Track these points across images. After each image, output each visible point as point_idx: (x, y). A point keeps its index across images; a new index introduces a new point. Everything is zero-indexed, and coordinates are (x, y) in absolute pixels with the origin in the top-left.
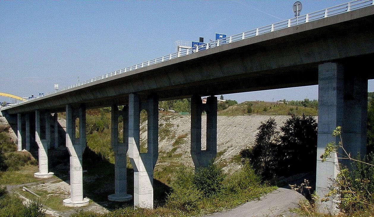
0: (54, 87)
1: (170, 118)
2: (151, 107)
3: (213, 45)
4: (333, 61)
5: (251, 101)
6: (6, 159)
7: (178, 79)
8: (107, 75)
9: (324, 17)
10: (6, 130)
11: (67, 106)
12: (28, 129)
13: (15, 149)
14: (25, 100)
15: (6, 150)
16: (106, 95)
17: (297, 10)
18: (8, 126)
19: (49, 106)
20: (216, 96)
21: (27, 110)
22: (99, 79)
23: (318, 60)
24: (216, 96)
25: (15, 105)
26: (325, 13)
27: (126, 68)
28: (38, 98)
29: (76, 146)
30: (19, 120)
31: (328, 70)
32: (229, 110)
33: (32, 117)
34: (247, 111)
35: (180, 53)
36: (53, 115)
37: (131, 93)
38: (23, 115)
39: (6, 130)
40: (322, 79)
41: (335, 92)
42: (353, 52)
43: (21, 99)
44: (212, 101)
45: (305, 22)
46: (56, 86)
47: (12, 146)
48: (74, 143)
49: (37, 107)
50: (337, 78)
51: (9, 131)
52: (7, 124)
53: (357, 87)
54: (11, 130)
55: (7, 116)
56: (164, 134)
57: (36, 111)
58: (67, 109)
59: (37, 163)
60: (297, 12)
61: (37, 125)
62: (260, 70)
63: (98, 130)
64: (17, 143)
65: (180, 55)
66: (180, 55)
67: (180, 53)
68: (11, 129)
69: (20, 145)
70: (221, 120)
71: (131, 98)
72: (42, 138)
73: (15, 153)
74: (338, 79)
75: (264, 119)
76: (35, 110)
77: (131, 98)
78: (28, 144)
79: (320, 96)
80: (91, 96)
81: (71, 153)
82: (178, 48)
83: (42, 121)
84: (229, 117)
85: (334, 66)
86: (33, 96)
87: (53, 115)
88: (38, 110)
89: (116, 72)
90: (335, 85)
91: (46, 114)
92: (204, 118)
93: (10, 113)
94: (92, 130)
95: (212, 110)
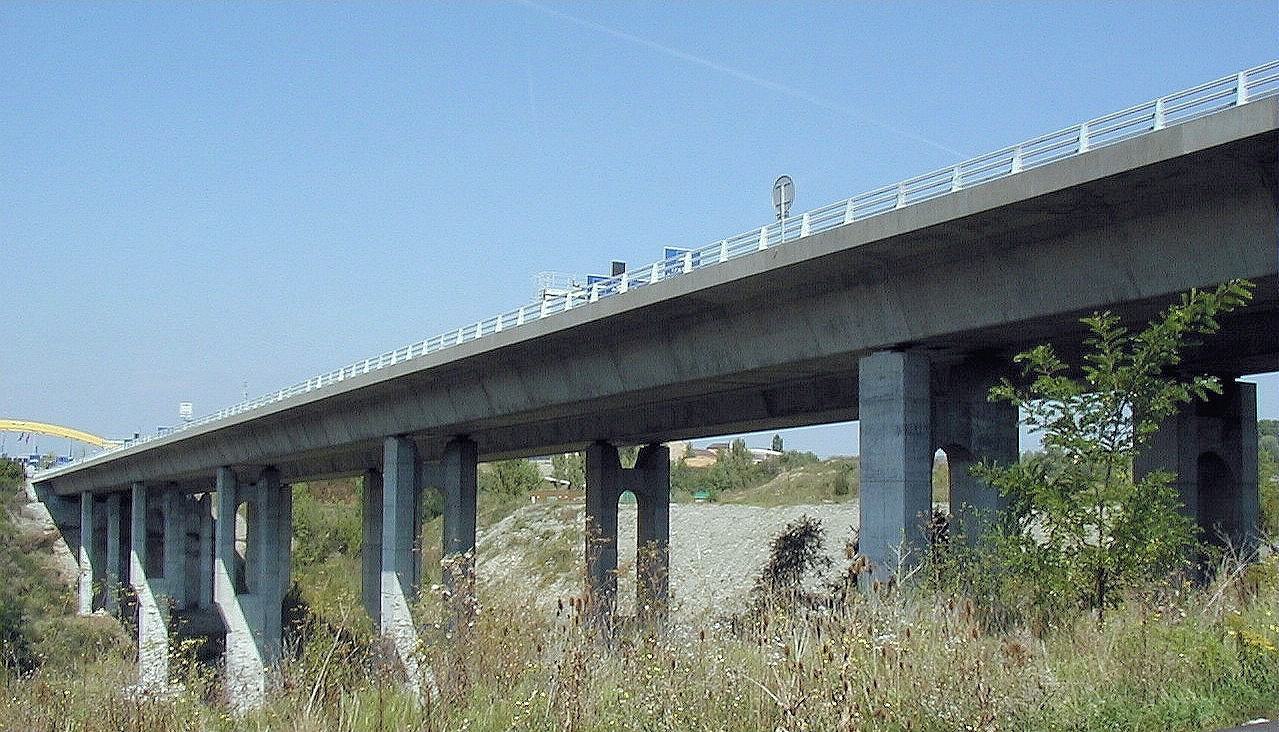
0: (194, 405)
1: (577, 512)
2: (453, 476)
3: (651, 277)
4: (899, 348)
5: (849, 455)
6: (39, 641)
7: (556, 390)
8: (480, 326)
9: (1152, 128)
10: (46, 545)
11: (220, 473)
12: (113, 542)
13: (71, 609)
14: (112, 448)
15: (40, 613)
16: (324, 442)
17: (783, 201)
18: (51, 532)
19: (170, 471)
20: (1244, 379)
21: (110, 481)
22: (300, 392)
23: (859, 346)
24: (1244, 379)
25: (90, 460)
26: (1081, 140)
27: (367, 361)
28: (150, 439)
29: (246, 598)
30: (86, 511)
31: (883, 377)
32: (778, 486)
33: (138, 504)
34: (832, 487)
35: (549, 304)
36: (198, 496)
37: (877, 349)
38: (100, 498)
39: (46, 545)
40: (868, 402)
41: (901, 438)
42: (944, 324)
43: (98, 441)
44: (654, 460)
45: (1152, 128)
46: (186, 409)
47: (61, 595)
48: (241, 588)
49: (135, 475)
50: (906, 399)
51: (55, 548)
52: (47, 526)
53: (983, 423)
54: (59, 546)
55: (52, 499)
56: (554, 565)
57: (83, 495)
58: (219, 483)
59: (131, 656)
60: (783, 206)
61: (138, 532)
62: (716, 373)
63: (344, 551)
64: (77, 589)
65: (549, 310)
66: (549, 310)
67: (549, 304)
68: (61, 541)
69: (86, 596)
70: (685, 516)
71: (391, 450)
72: (153, 571)
73: (68, 620)
74: (911, 401)
75: (791, 516)
76: (217, 467)
77: (391, 450)
78: (113, 595)
79: (865, 450)
80: (307, 441)
81: (230, 623)
82: (538, 287)
83: (155, 516)
84: (768, 507)
85: (897, 361)
86: (137, 436)
87: (198, 496)
88: (140, 483)
89: (342, 372)
90: (900, 420)
91: (167, 496)
92: (628, 511)
93: (62, 490)
94: (326, 549)
95: (654, 487)
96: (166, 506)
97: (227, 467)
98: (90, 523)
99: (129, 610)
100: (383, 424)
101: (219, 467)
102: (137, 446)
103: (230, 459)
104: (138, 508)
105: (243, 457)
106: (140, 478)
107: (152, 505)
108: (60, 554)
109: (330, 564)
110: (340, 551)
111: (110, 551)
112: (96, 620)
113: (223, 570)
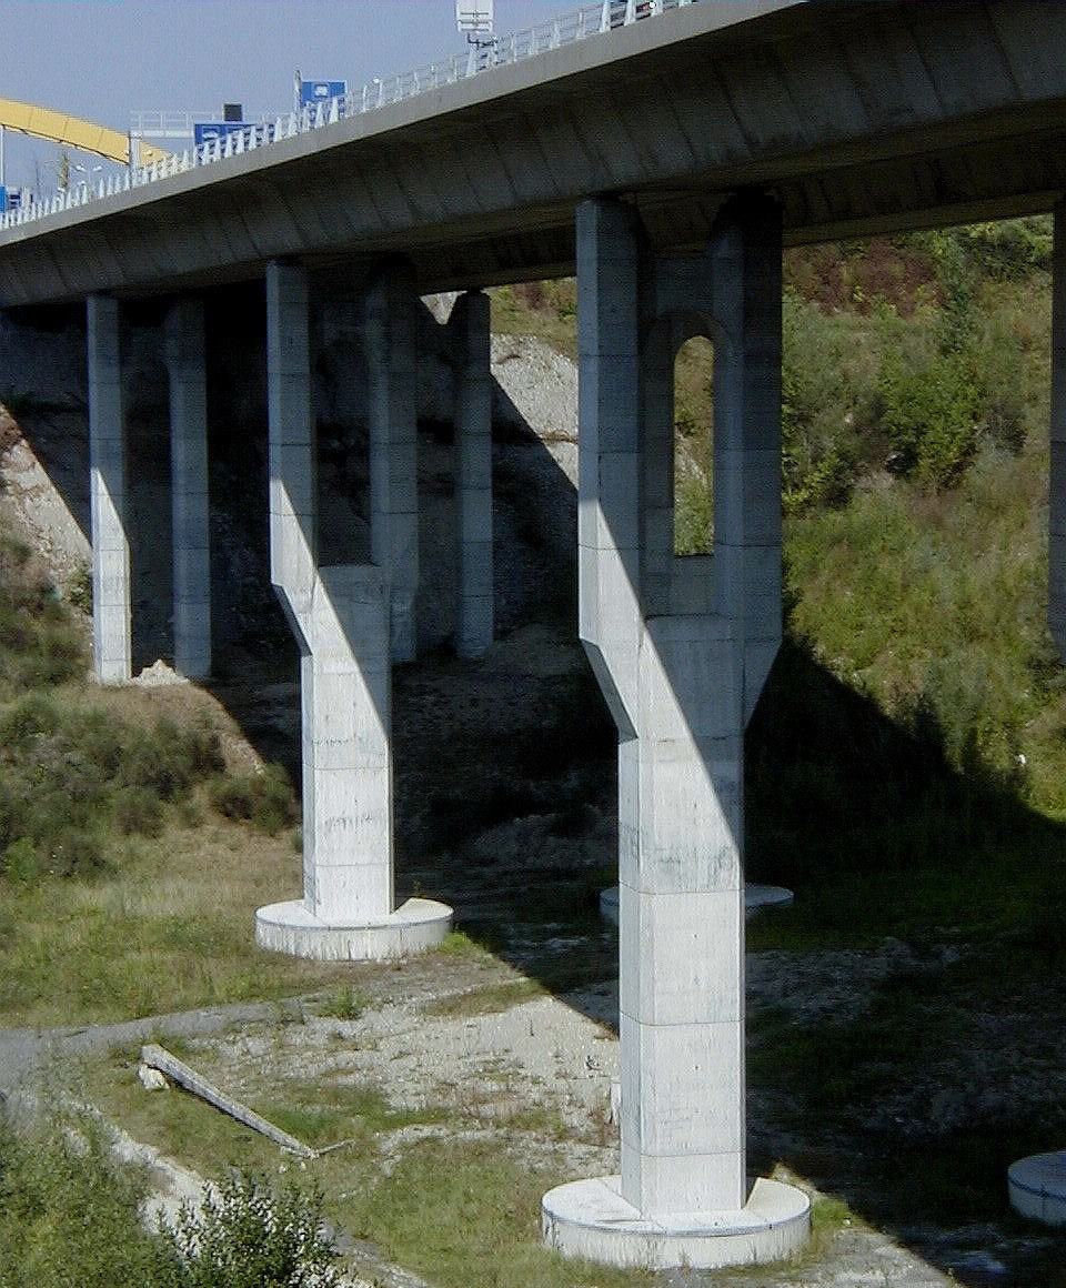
11: (588, 219)
12: (189, 452)
13: (68, 662)
14: (156, 160)
19: (400, 216)
21: (182, 258)
29: (683, 631)
38: (142, 311)
49: (279, 233)
57: (273, 275)
59: (279, 807)
63: (904, 466)
68: (21, 453)
73: (63, 700)
81: (631, 708)
83: (330, 370)
87: (442, 305)
88: (288, 260)
94: (849, 464)
96: (373, 331)
97: (608, 198)
98: (115, 392)
99: (254, 659)
100: (279, 233)
101: (581, 198)
102: (232, 156)
103: (623, 166)
104: (286, 341)
105: (674, 159)
106: (291, 241)
107: (330, 332)
108: (22, 493)
109: (863, 509)
110: (889, 468)
111: (180, 480)
112: (150, 695)
113: (604, 537)
